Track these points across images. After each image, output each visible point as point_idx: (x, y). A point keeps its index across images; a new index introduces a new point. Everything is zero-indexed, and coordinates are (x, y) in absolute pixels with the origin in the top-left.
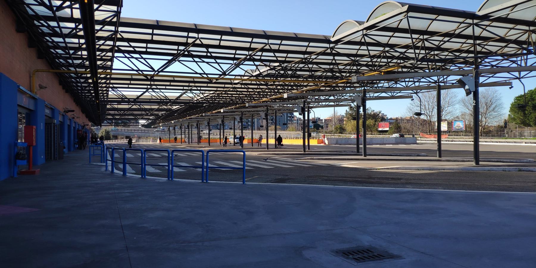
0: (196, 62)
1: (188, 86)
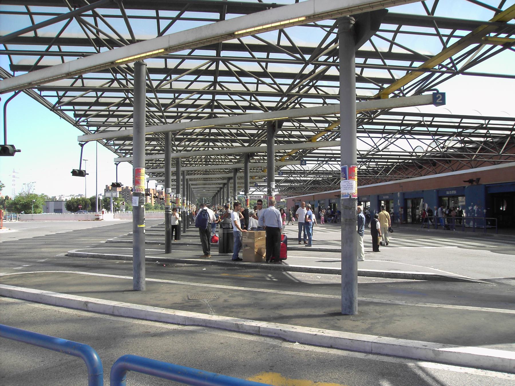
0: (407, 139)
1: (317, 161)
